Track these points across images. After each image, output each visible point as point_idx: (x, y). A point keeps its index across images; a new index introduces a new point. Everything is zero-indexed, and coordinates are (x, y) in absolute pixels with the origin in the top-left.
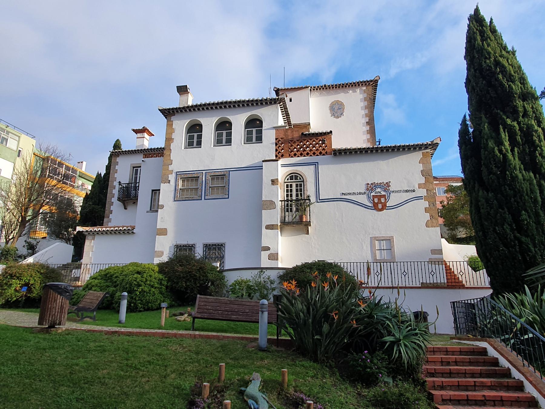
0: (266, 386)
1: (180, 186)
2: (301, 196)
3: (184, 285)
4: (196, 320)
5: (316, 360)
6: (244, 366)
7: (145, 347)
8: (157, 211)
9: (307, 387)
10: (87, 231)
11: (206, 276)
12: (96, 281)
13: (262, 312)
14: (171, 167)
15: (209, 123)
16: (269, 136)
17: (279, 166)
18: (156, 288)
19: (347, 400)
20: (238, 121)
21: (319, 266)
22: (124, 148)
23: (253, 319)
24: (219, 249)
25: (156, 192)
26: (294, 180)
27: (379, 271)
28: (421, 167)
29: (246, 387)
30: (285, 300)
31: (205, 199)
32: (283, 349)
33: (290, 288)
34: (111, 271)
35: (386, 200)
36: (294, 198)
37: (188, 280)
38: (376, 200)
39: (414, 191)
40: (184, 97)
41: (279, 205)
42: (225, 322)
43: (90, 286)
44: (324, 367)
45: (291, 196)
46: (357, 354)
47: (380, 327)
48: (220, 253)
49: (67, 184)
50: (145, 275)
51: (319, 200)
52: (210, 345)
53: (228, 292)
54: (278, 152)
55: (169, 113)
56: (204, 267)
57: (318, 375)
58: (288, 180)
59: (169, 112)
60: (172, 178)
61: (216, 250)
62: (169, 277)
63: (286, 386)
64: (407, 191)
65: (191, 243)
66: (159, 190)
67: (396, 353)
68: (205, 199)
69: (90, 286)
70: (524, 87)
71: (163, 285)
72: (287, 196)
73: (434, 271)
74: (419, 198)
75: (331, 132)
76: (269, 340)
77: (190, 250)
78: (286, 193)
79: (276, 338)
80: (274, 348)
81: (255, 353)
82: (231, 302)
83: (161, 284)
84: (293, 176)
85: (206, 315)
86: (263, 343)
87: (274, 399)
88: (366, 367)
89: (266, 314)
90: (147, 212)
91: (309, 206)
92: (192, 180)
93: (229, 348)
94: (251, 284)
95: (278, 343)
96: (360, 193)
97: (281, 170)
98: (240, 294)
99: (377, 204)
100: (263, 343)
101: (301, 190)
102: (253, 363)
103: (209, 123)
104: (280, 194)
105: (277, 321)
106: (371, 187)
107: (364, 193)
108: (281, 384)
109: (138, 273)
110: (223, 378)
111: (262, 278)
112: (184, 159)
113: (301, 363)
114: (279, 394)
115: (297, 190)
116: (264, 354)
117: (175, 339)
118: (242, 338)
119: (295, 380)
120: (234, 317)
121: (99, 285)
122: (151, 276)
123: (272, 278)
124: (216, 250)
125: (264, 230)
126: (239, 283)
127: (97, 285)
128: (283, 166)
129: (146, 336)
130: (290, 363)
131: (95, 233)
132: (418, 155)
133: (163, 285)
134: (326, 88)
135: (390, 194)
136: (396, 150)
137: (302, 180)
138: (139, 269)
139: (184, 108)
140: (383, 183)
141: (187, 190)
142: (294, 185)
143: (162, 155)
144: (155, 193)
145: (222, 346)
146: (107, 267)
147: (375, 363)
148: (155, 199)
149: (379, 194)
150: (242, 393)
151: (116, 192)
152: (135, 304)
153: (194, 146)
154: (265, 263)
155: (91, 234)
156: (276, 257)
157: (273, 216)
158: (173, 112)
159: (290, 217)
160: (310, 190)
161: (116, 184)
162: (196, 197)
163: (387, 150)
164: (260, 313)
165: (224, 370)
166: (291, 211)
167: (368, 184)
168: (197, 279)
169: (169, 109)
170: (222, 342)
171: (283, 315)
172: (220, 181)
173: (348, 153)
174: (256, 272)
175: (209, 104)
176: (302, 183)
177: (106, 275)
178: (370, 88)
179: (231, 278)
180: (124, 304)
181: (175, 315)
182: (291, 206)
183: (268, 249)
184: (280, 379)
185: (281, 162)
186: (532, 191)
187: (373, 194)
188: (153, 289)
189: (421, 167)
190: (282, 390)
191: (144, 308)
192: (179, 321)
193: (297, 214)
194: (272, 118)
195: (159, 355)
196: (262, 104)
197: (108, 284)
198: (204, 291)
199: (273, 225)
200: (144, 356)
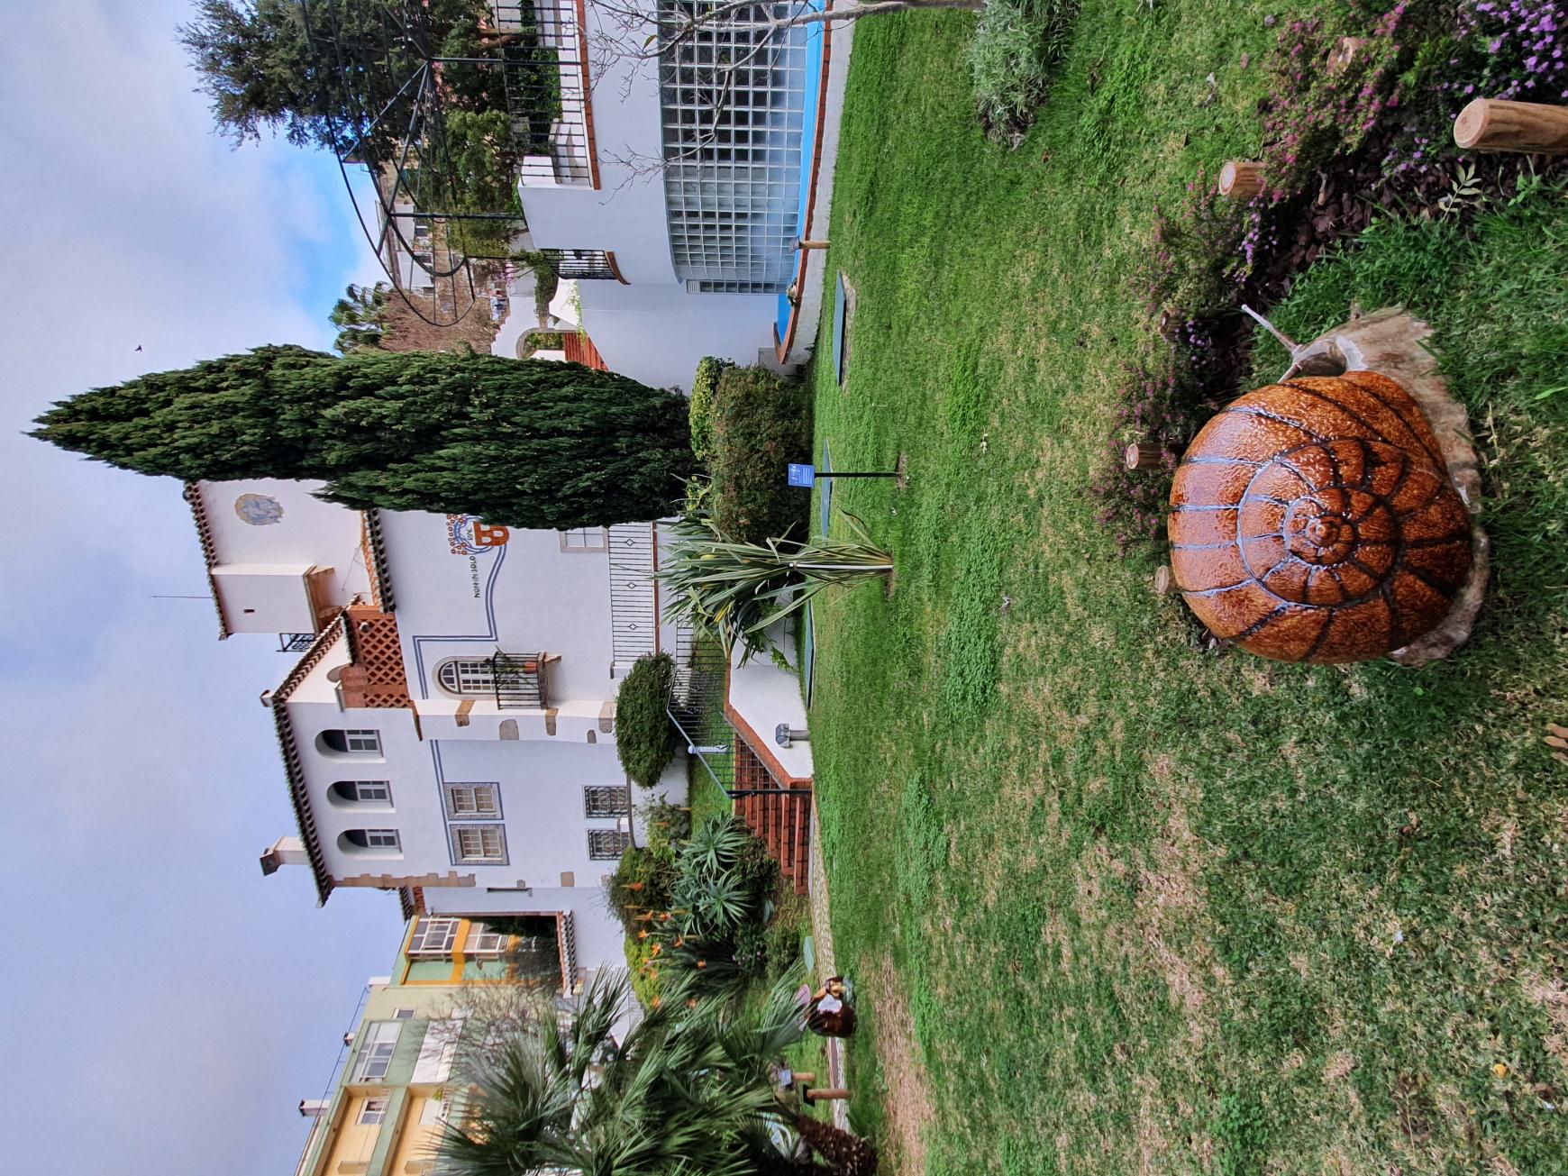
1: (474, 812)
45: (486, 682)
51: (493, 636)
60: (463, 872)
65: (585, 837)
70: (243, 410)
104: (485, 707)
142: (463, 676)
162: (499, 833)
186: (477, 459)
187: (473, 543)
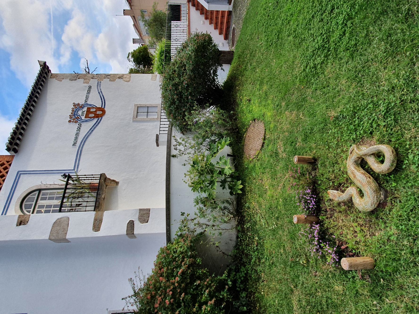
39: (90, 87)
72: (101, 82)
106: (74, 118)
125: (103, 232)
135: (88, 104)
149: (85, 113)
183: (131, 225)
187: (83, 118)
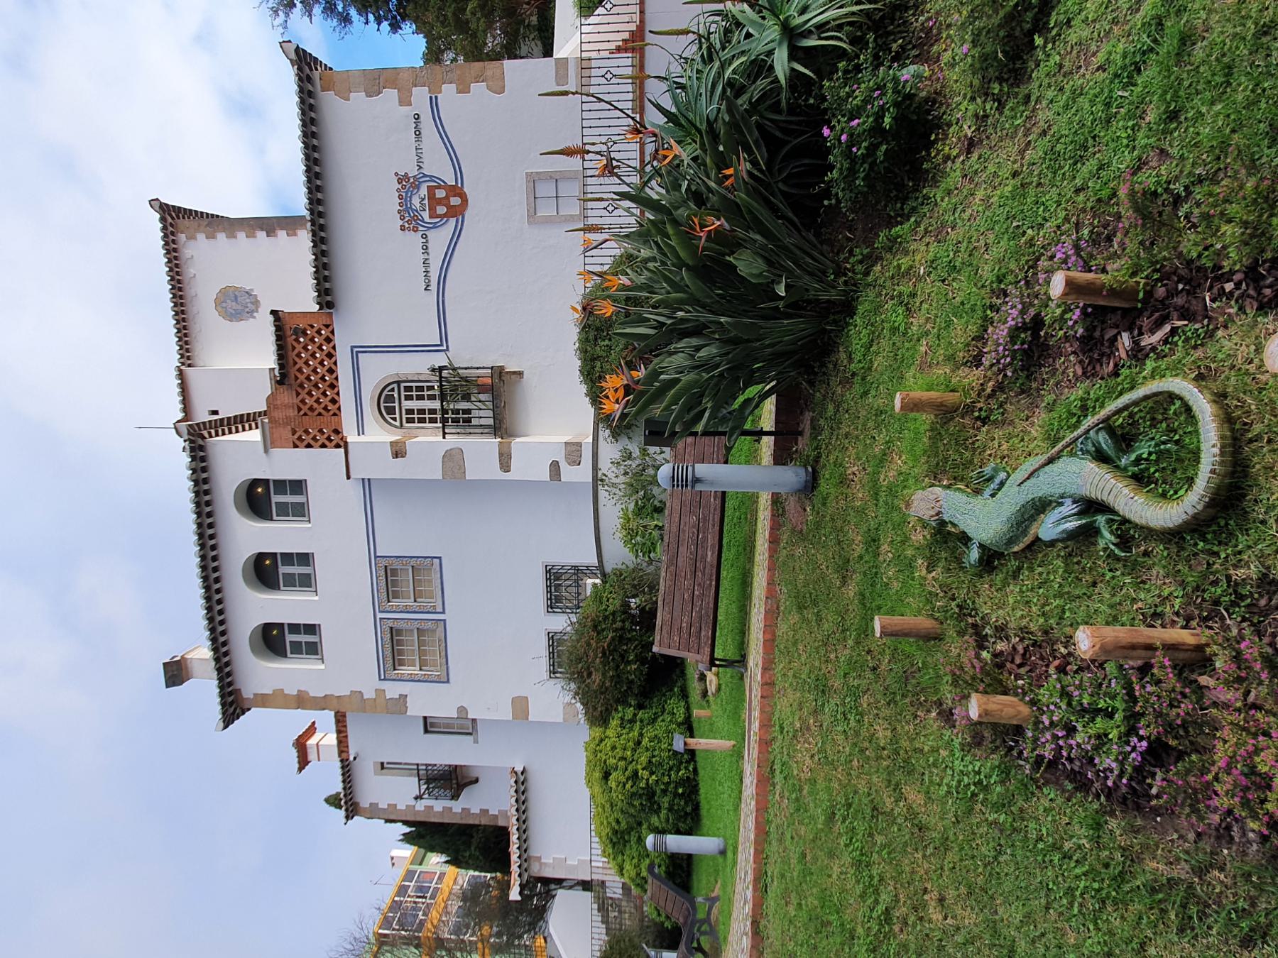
0: (956, 464)
2: (433, 388)
3: (634, 667)
4: (719, 653)
5: (847, 308)
6: (873, 541)
7: (804, 855)
8: (474, 720)
9: (949, 324)
10: (520, 876)
11: (614, 614)
12: (627, 866)
13: (697, 480)
14: (369, 694)
15: (254, 607)
16: (287, 463)
17: (362, 439)
18: (641, 735)
19: (1005, 173)
20: (247, 537)
21: (587, 340)
22: (337, 787)
23: (714, 503)
24: (557, 579)
25: (429, 726)
26: (396, 405)
27: (605, 204)
28: (358, 97)
29: (965, 539)
30: (657, 411)
31: (443, 612)
32: (808, 415)
33: (621, 393)
34: (603, 834)
35: (439, 187)
36: (436, 405)
37: (622, 656)
38: (441, 210)
39: (417, 117)
40: (196, 668)
41: (453, 441)
42: (724, 574)
43: (638, 881)
44: (870, 279)
45: (433, 411)
46: (831, 168)
47: (743, 102)
48: (567, 576)
49: (436, 890)
50: (612, 761)
51: (443, 344)
52: (795, 643)
53: (651, 562)
54: (327, 443)
55: (233, 706)
56: (593, 620)
57: (900, 294)
58: (395, 419)
59: (231, 704)
60: (393, 690)
61: (558, 583)
62: (618, 701)
63: (952, 398)
64: (418, 133)
65: (544, 642)
66: (425, 718)
67: (827, 38)
68: (443, 612)
69: (638, 881)
71: (635, 715)
72: (433, 421)
73: (603, 72)
74: (434, 103)
75: (273, 313)
76: (781, 457)
77: (560, 642)
78: (427, 425)
79: (768, 441)
80: (803, 443)
81: (824, 504)
82: (673, 560)
83: (632, 721)
84: (387, 404)
85: (706, 633)
86: (791, 476)
87: (1009, 437)
88: (876, 129)
89: (702, 469)
90: (476, 741)
91: (454, 369)
92: (400, 643)
93: (806, 585)
94: (632, 506)
95: (786, 435)
96: (425, 248)
97: (370, 436)
98: (656, 533)
99: (449, 207)
100: (791, 476)
101: (420, 389)
102: (861, 512)
103: (254, 607)
105: (724, 434)
106: (410, 220)
107: (424, 236)
108: (946, 413)
109: (606, 776)
110: (924, 623)
111: (617, 481)
112: (350, 661)
113: (857, 357)
114: (985, 421)
115: (420, 398)
116: (825, 473)
117: (776, 745)
118: (774, 540)
119: (926, 366)
120: (710, 557)
121: (635, 861)
122: (614, 748)
123: (617, 456)
124: (558, 583)
126: (630, 534)
127: (637, 866)
128: (361, 430)
129: (767, 833)
130: (858, 388)
131: (525, 856)
132: (329, 102)
133: (635, 715)
134: (185, 328)
135: (425, 176)
136: (316, 155)
137: (395, 386)
138: (597, 775)
139: (219, 670)
140: (398, 190)
141: (422, 653)
143: (344, 716)
144: (433, 725)
145: (801, 608)
146: (597, 839)
147: (859, 105)
148: (447, 726)
149: (426, 202)
150: (991, 559)
151: (439, 805)
152: (678, 785)
153: (379, 616)
154: (580, 474)
155: (525, 865)
156: (574, 448)
157: (479, 451)
158: (230, 694)
159: (482, 413)
160: (418, 366)
161: (420, 806)
163: (318, 176)
164: (699, 487)
165: (896, 621)
166: (468, 411)
167: (403, 228)
168: (621, 637)
169: (223, 705)
170: (785, 602)
171: (707, 414)
172: (396, 578)
173: (326, 273)
174: (602, 494)
175: (209, 609)
176: (403, 385)
177: (614, 844)
178: (183, 223)
179: (619, 554)
180: (677, 843)
181: (705, 694)
182: (457, 412)
184: (925, 420)
185: (352, 438)
187: (426, 215)
188: (645, 742)
189: (358, 97)
190: (969, 409)
191: (688, 762)
192: (719, 689)
193: (470, 398)
194: (243, 457)
195: (831, 817)
196: (206, 481)
197: (634, 839)
198: (647, 618)
199: (501, 455)
200: (836, 870)
